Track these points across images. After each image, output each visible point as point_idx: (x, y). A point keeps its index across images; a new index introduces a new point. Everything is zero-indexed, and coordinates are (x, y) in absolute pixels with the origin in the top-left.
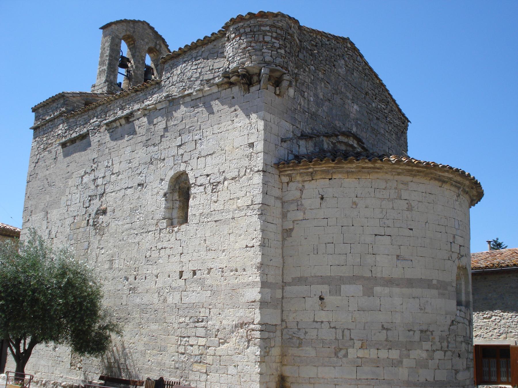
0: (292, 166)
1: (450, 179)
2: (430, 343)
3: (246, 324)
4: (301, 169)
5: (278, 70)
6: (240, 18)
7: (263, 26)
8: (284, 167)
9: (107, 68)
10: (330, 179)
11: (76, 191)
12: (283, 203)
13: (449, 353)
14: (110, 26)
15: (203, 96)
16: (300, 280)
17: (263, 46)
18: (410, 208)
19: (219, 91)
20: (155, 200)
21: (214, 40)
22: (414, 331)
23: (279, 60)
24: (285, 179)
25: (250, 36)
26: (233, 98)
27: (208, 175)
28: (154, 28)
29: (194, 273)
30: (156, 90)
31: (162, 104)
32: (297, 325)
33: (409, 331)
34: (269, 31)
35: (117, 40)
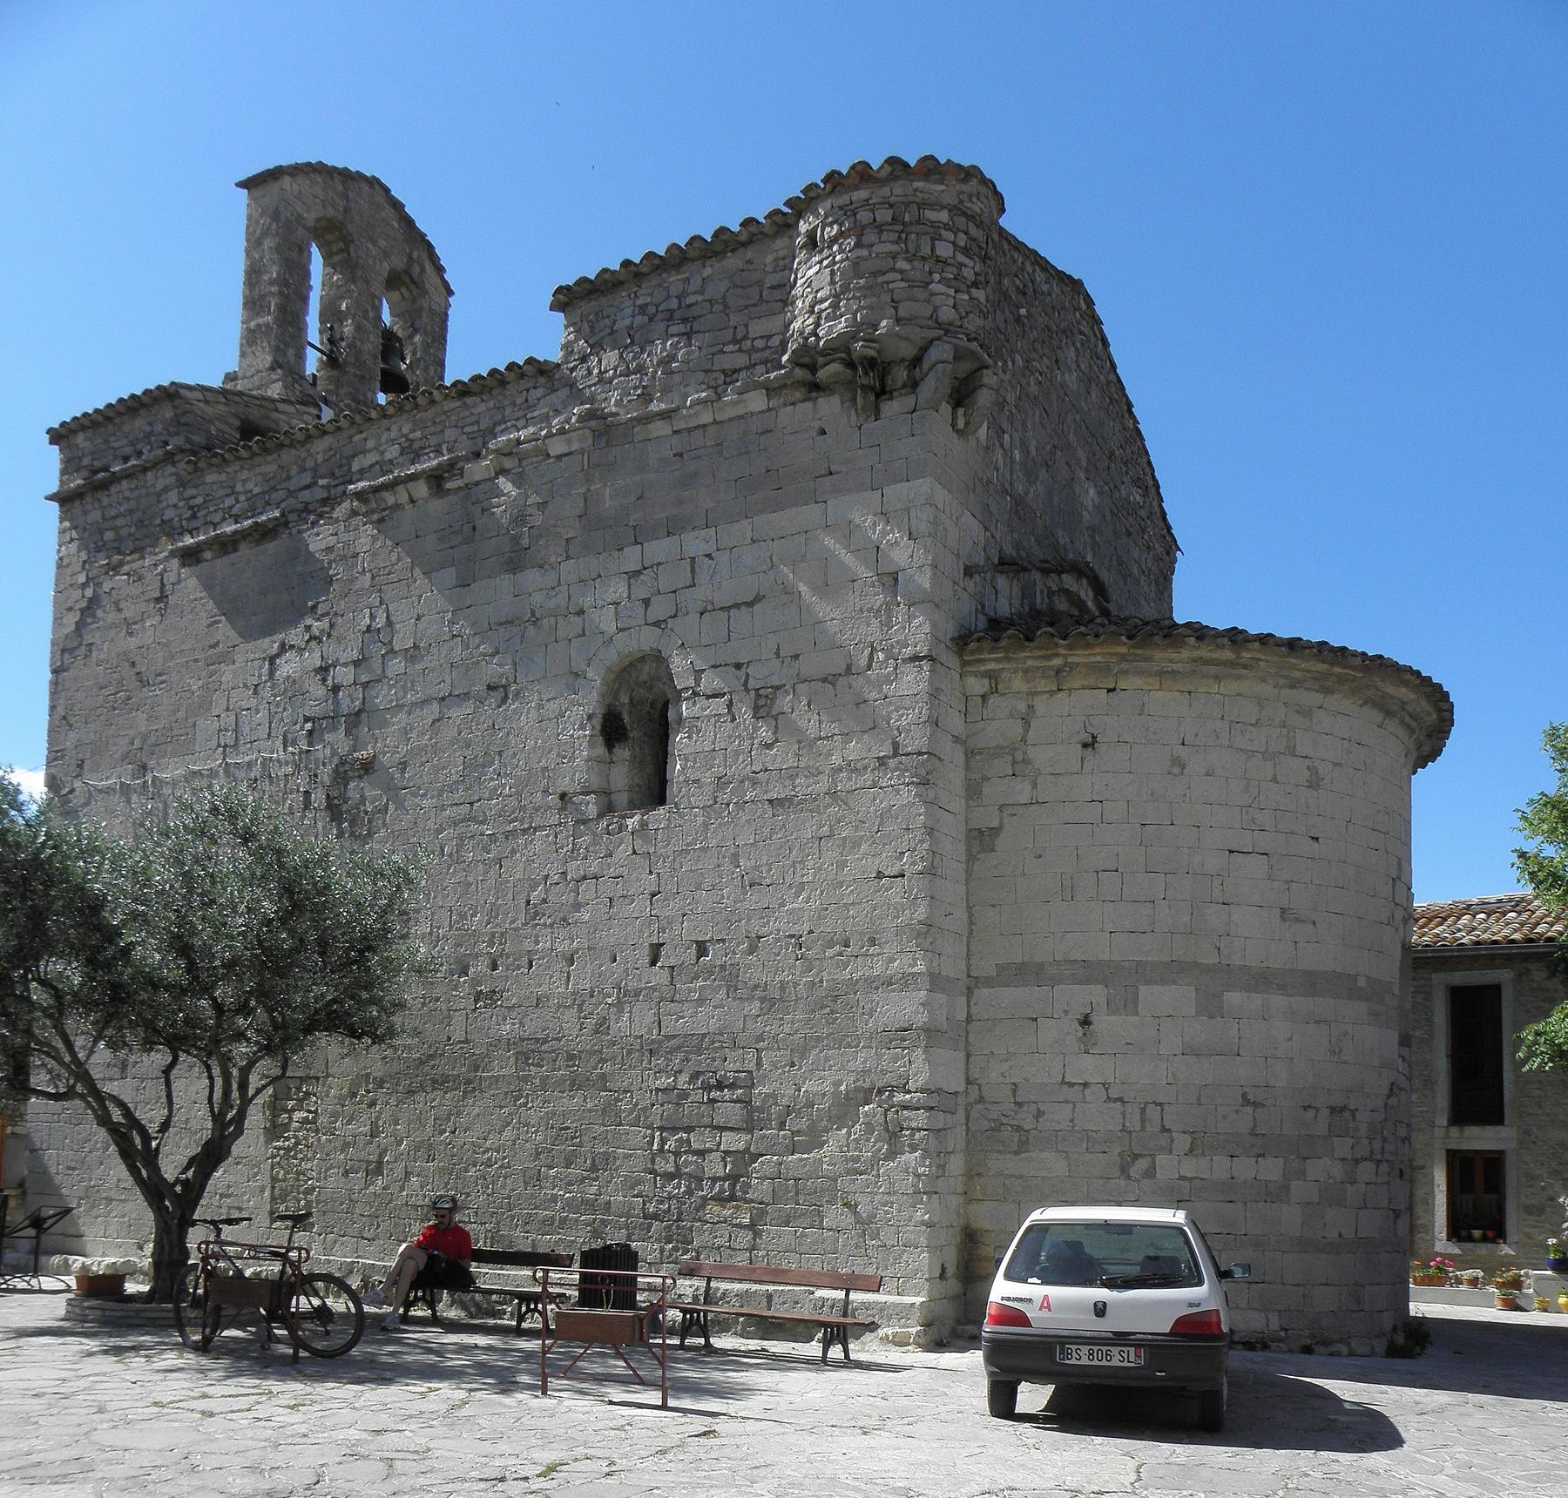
0: (1006, 649)
1: (1403, 704)
2: (1350, 1141)
3: (880, 1092)
4: (1029, 658)
5: (973, 353)
6: (862, 172)
7: (932, 206)
8: (980, 650)
9: (276, 319)
10: (1110, 691)
11: (253, 702)
12: (970, 754)
13: (1384, 1167)
14: (276, 179)
15: (715, 422)
16: (1024, 973)
17: (931, 273)
18: (1314, 783)
19: (769, 410)
20: (556, 733)
21: (743, 245)
22: (1317, 1109)
23: (974, 323)
24: (977, 686)
25: (894, 236)
26: (823, 432)
27: (738, 666)
28: (403, 206)
29: (702, 949)
30: (539, 392)
31: (569, 442)
32: (1014, 1092)
33: (1305, 1108)
34: (946, 227)
35: (300, 231)
